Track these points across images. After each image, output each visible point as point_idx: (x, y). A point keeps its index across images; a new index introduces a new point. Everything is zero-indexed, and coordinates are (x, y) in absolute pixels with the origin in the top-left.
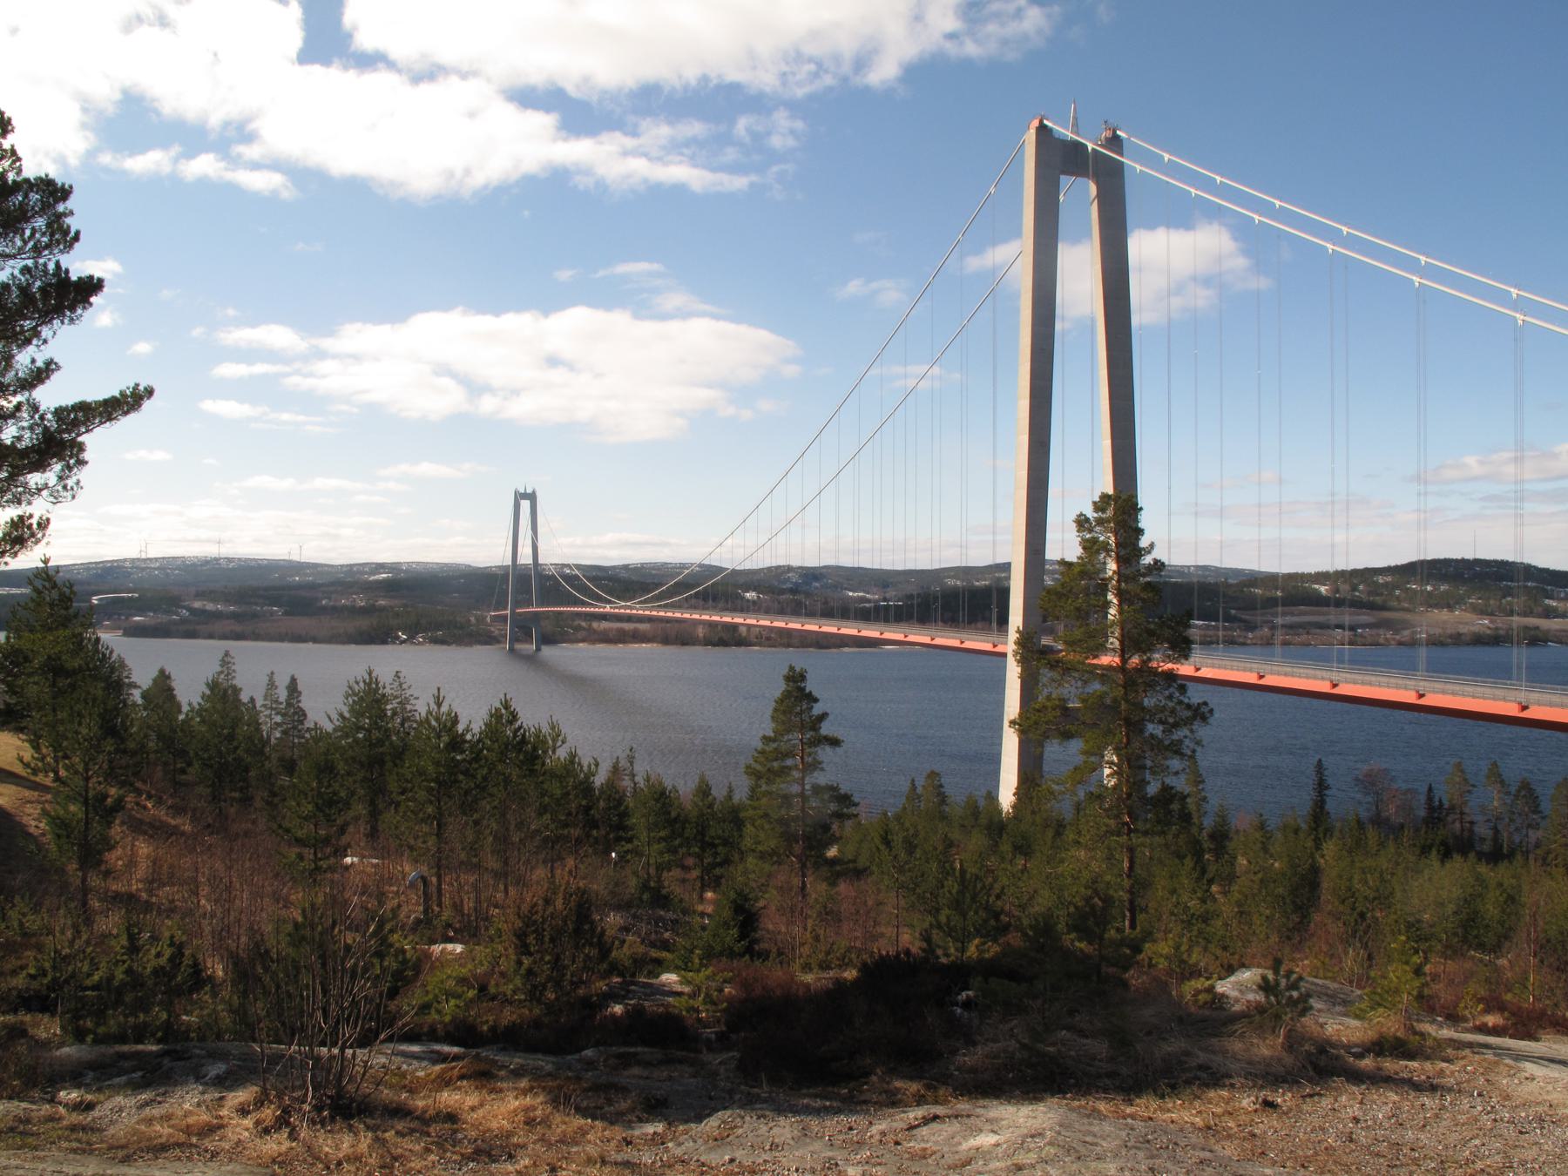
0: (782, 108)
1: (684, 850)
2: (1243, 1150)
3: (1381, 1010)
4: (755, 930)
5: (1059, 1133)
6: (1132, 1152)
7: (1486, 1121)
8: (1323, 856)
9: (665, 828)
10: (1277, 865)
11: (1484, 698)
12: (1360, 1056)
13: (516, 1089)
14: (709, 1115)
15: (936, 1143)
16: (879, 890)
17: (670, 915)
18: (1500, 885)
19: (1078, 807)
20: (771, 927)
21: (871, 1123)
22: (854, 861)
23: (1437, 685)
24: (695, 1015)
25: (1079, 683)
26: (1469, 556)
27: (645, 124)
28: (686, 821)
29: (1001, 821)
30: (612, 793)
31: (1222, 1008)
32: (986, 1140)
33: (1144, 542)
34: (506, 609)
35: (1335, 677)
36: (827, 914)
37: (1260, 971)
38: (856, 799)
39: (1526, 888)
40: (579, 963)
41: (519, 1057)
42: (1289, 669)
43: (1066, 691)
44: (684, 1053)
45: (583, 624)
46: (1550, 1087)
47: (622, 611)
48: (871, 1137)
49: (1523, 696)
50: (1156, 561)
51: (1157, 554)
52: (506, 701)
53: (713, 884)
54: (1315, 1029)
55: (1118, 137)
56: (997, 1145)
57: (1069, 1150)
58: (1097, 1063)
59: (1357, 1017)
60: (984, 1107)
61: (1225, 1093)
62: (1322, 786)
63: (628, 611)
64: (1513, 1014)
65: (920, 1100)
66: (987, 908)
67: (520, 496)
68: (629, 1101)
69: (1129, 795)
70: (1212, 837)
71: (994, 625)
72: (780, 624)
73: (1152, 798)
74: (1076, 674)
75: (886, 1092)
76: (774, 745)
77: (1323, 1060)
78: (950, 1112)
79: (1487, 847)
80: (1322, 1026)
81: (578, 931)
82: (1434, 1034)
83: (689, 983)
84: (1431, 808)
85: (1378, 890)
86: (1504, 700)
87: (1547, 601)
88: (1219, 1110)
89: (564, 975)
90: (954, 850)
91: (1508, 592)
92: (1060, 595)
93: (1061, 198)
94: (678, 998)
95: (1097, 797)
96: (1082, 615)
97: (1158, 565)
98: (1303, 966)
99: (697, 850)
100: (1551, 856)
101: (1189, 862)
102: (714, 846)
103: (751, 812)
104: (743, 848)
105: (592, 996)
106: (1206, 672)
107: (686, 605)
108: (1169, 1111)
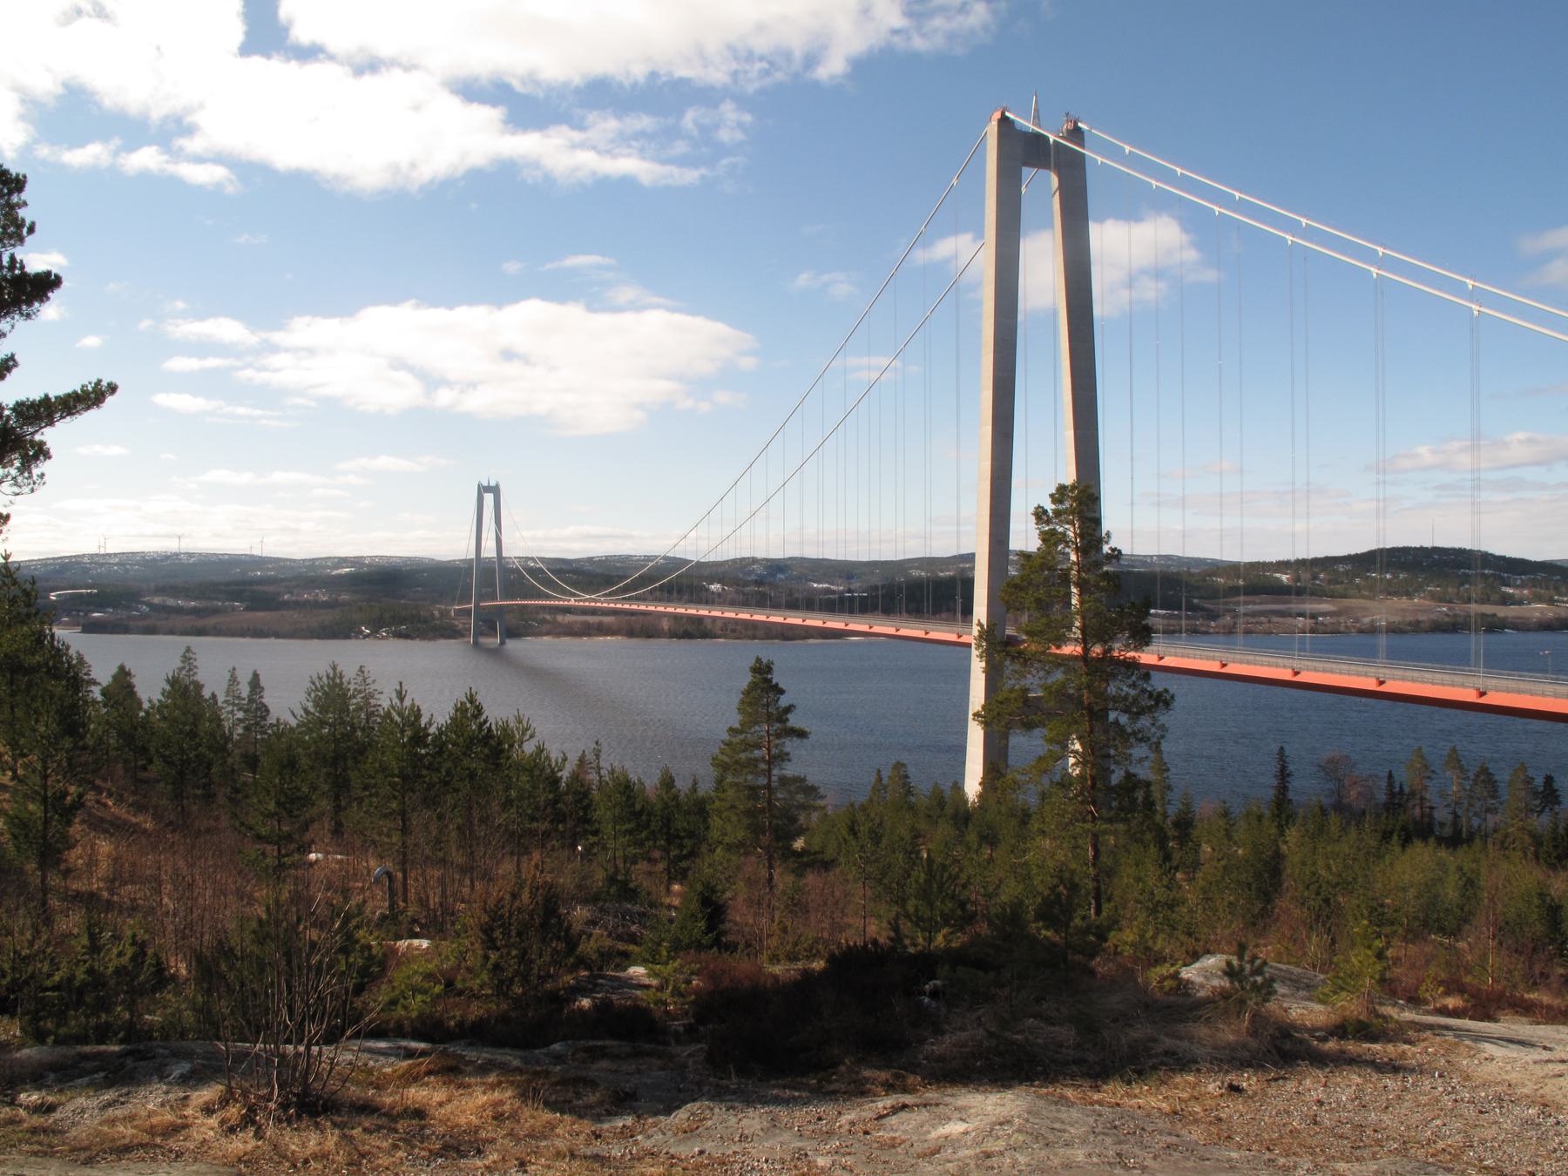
2: (1210, 1135)
7: (1447, 1101)
11: (1443, 685)
12: (1324, 1040)
13: (484, 1084)
14: (679, 1107)
15: (905, 1132)
17: (637, 908)
19: (1044, 796)
20: (738, 919)
21: (840, 1113)
23: (1399, 673)
26: (1428, 544)
31: (1187, 995)
32: (955, 1128)
35: (1297, 664)
38: (822, 791)
39: (1484, 871)
40: (547, 958)
44: (652, 1046)
45: (548, 617)
46: (1509, 1067)
47: (587, 604)
48: (840, 1127)
52: (471, 695)
53: (679, 877)
56: (966, 1133)
57: (1037, 1137)
58: (1064, 1050)
59: (1321, 1002)
60: (953, 1095)
61: (1191, 1078)
62: (1284, 774)
63: (593, 604)
65: (890, 1088)
66: (953, 897)
67: (483, 490)
70: (1176, 824)
71: (959, 615)
77: (1288, 1046)
78: (918, 1101)
80: (1286, 1011)
82: (1396, 1016)
83: (656, 975)
84: (1392, 795)
86: (1463, 686)
88: (1185, 1095)
94: (645, 991)
95: (1065, 783)
97: (1116, 554)
99: (663, 842)
101: (1153, 850)
106: (1169, 661)
108: (1136, 1096)
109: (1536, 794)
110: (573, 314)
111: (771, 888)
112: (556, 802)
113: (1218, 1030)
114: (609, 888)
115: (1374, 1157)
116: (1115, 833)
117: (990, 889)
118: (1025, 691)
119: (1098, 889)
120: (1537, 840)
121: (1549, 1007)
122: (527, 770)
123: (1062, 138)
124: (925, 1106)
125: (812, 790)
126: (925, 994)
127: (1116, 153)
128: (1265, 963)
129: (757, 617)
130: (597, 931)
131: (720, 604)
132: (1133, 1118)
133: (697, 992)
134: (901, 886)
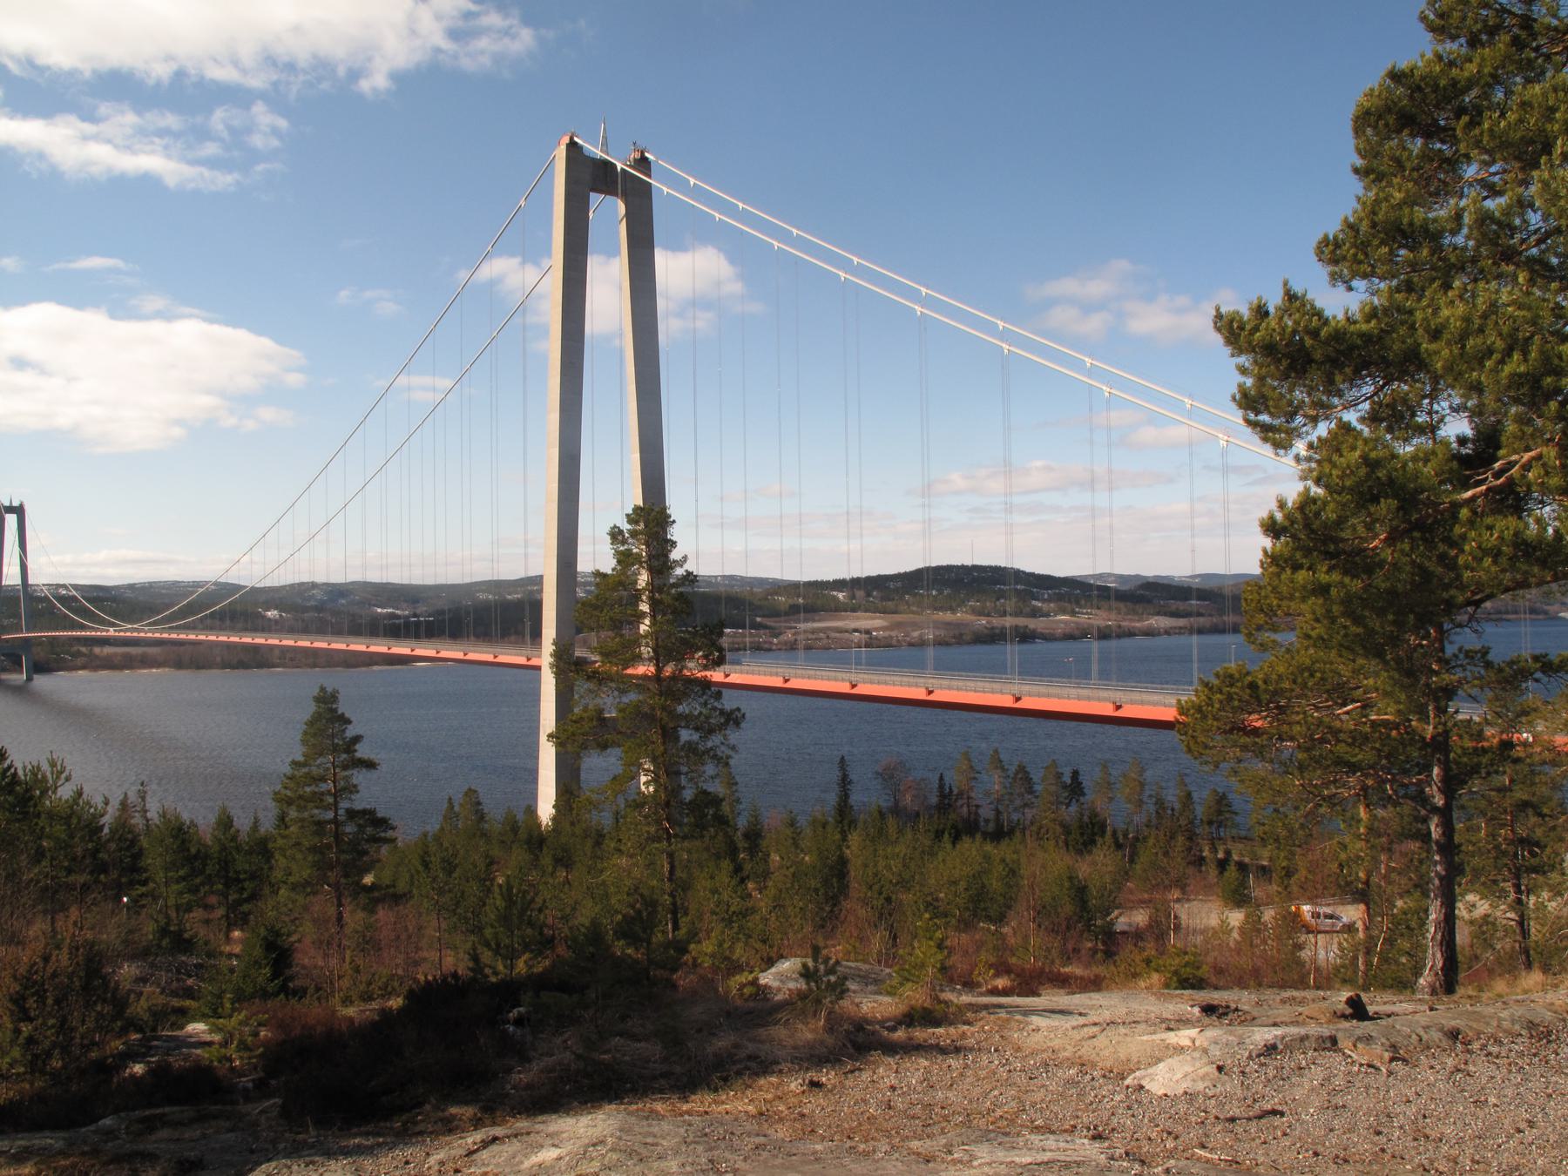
0: (260, 103)
1: (207, 888)
2: (794, 1131)
3: (910, 984)
5: (620, 1138)
6: (691, 1147)
9: (183, 866)
10: (807, 858)
12: (893, 1029)
15: (498, 1165)
18: (1003, 860)
21: (428, 1154)
22: (394, 886)
24: (228, 1065)
25: (616, 693)
26: (968, 562)
27: (104, 109)
30: (126, 837)
32: (548, 1155)
33: (675, 555)
35: (854, 678)
36: (367, 943)
39: (1023, 860)
40: (90, 1024)
41: (22, 1139)
42: (812, 672)
43: (601, 702)
44: (218, 1107)
45: (83, 649)
46: (1052, 1035)
47: (128, 634)
48: (429, 1168)
49: (1016, 689)
50: (689, 574)
51: (690, 566)
54: (852, 1009)
56: (560, 1158)
57: (630, 1153)
58: (651, 1064)
59: (889, 994)
60: (543, 1122)
61: (774, 1079)
62: (845, 782)
63: (135, 634)
64: (1018, 975)
65: (477, 1124)
70: (746, 836)
72: (305, 643)
74: (613, 685)
75: (441, 1120)
76: (305, 770)
77: (860, 1038)
78: (509, 1132)
79: (991, 827)
80: (857, 1005)
81: (86, 988)
82: (956, 1001)
83: (218, 1029)
84: (942, 796)
86: (1001, 692)
87: (1034, 602)
88: (769, 1096)
89: (72, 1038)
90: (495, 867)
91: (1001, 595)
93: (591, 215)
94: (207, 1048)
95: (639, 803)
97: (690, 578)
98: (836, 951)
99: (220, 887)
100: (1043, 831)
101: (726, 864)
102: (238, 880)
103: (280, 842)
104: (273, 881)
105: (106, 1058)
106: (735, 678)
108: (723, 1103)
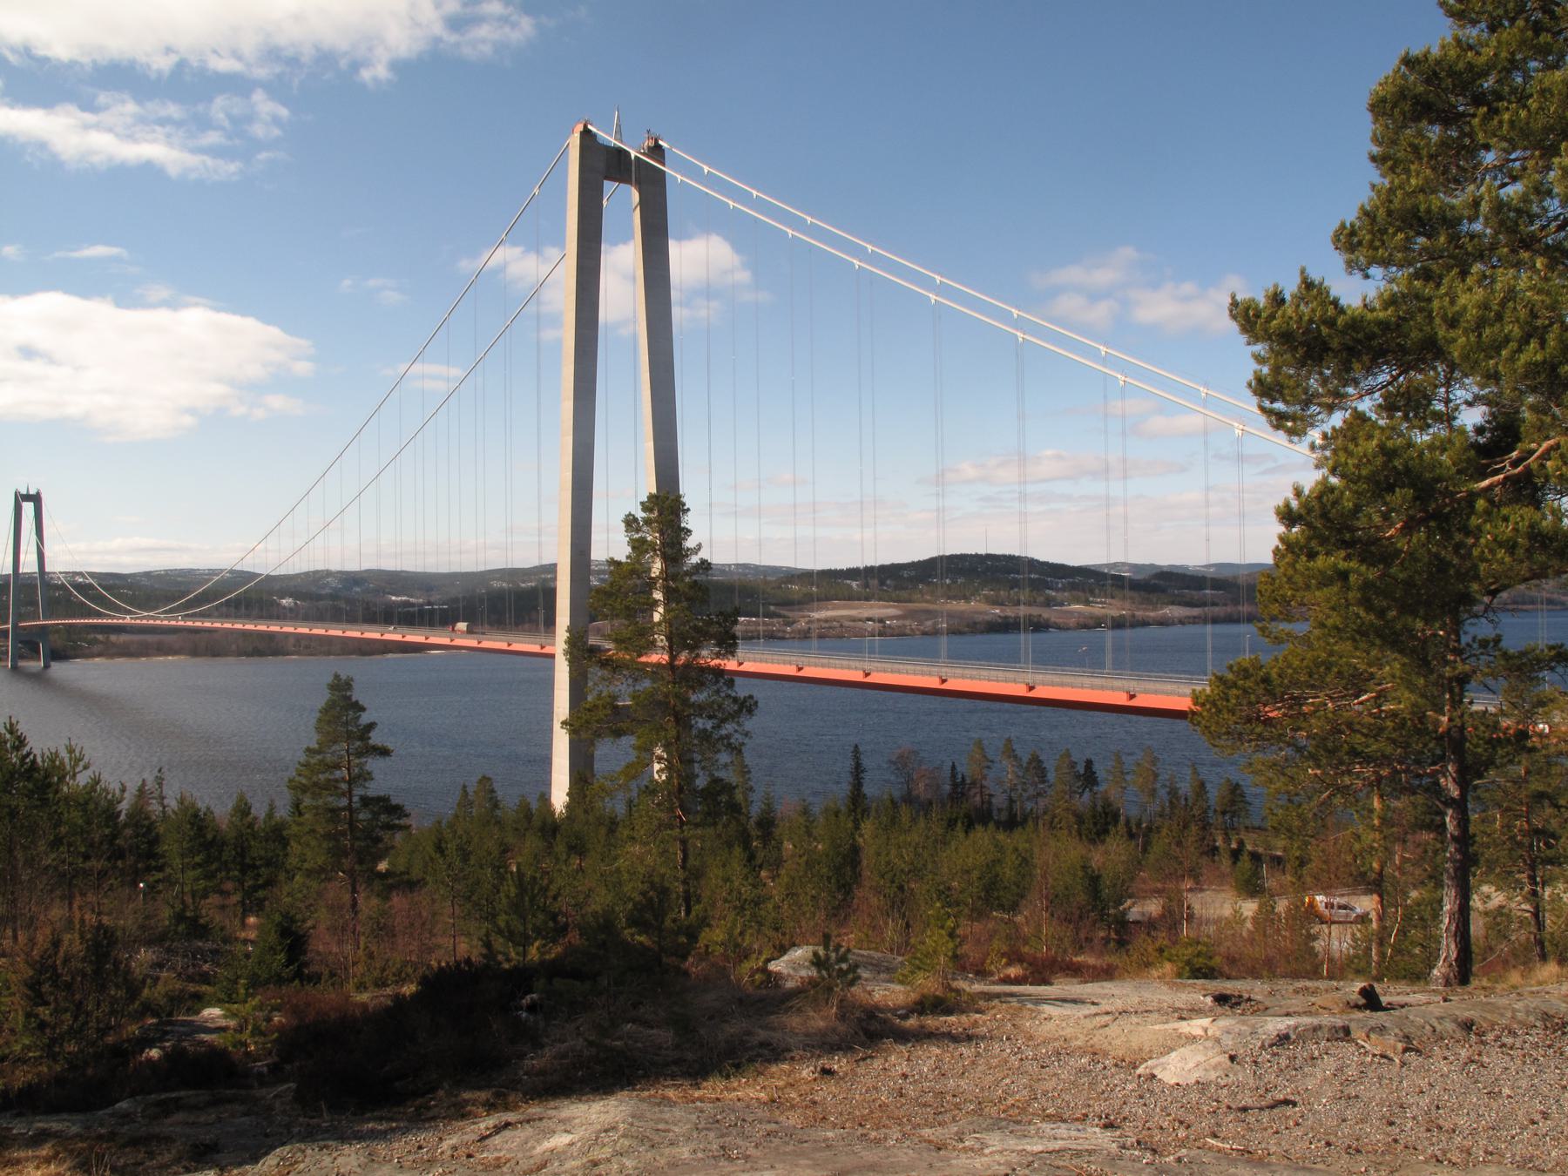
1: (224, 873)
2: (806, 1118)
4: (305, 953)
7: (1014, 1061)
8: (861, 835)
9: (200, 852)
11: (997, 681)
12: (905, 1017)
13: (37, 1157)
14: (266, 1154)
15: (510, 1150)
16: (434, 901)
17: (209, 945)
18: (1016, 849)
19: (630, 803)
20: (321, 948)
21: (441, 1139)
23: (959, 671)
26: (982, 551)
28: (224, 843)
29: (554, 821)
30: (139, 817)
31: (777, 986)
32: (560, 1140)
33: (690, 543)
34: (6, 622)
35: (867, 666)
37: (811, 948)
38: (408, 809)
39: (1036, 850)
40: (105, 1007)
44: (233, 1091)
46: (1064, 1024)
47: (145, 622)
48: (442, 1153)
50: (703, 562)
52: (11, 725)
53: (255, 908)
55: (660, 147)
56: (571, 1144)
57: (642, 1140)
58: (663, 1052)
59: (901, 982)
60: (556, 1108)
61: (785, 1067)
62: (858, 771)
63: (151, 622)
65: (491, 1107)
66: (544, 910)
67: (20, 498)
68: (174, 1151)
69: (681, 790)
70: (760, 824)
71: (542, 627)
73: (702, 790)
75: (454, 1105)
76: (319, 757)
77: (875, 1026)
78: (521, 1117)
79: (1004, 816)
80: (869, 993)
82: (968, 989)
83: (234, 1015)
84: (955, 785)
85: (912, 864)
86: (1015, 681)
87: (1048, 592)
88: (781, 1083)
92: (608, 594)
93: (605, 203)
94: (223, 1034)
95: (651, 789)
96: (630, 613)
97: (705, 565)
98: (849, 938)
99: (236, 873)
101: (737, 850)
102: (254, 867)
103: (295, 828)
106: (748, 667)
107: (216, 614)
108: (735, 1090)
109: (1078, 777)
110: (100, 311)
111: (356, 913)
112: (114, 836)
113: (808, 1018)
114: (177, 925)
115: (954, 1120)
116: (702, 838)
117: (581, 898)
118: (614, 698)
119: (687, 892)
120: (1080, 819)
121: (1094, 967)
122: (80, 804)
123: (644, 154)
124: (528, 1121)
125: (397, 810)
126: (521, 1009)
127: (696, 173)
128: (849, 950)
129: (332, 632)
130: (164, 974)
131: (292, 619)
132: (733, 1111)
133: (281, 1029)
134: (490, 902)
